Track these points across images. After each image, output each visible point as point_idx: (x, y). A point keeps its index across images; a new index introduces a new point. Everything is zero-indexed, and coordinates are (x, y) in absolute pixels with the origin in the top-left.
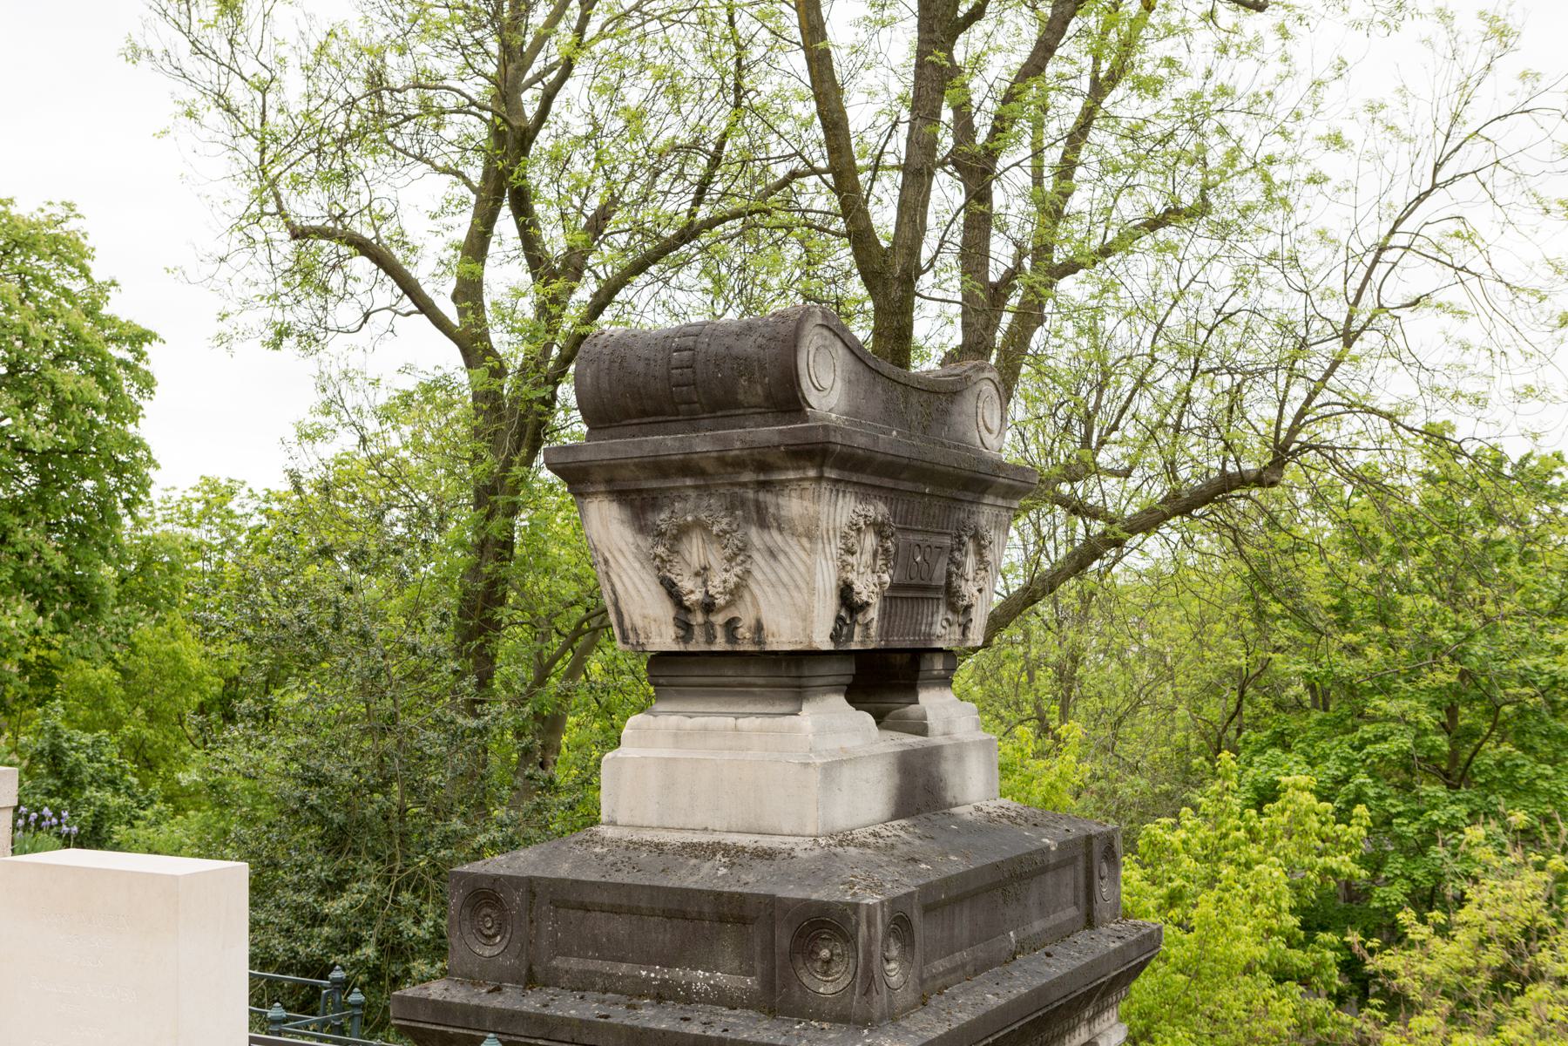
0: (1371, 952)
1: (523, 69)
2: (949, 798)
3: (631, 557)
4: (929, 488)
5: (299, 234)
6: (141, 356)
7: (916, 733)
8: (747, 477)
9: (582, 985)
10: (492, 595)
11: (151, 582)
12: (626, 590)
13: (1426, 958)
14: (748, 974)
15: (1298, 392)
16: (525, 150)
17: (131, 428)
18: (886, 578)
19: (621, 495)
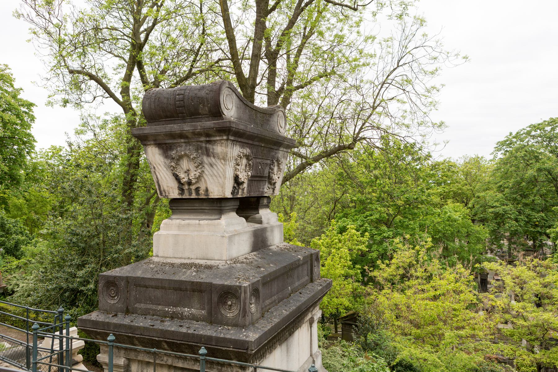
0: (371, 271)
1: (140, 26)
2: (269, 244)
3: (163, 166)
4: (262, 143)
5: (71, 72)
6: (30, 110)
7: (259, 223)
8: (203, 139)
9: (145, 313)
10: (133, 180)
11: (34, 174)
12: (161, 178)
13: (383, 272)
14: (203, 309)
15: (360, 123)
16: (141, 50)
17: (28, 131)
18: (250, 173)
19: (159, 145)
